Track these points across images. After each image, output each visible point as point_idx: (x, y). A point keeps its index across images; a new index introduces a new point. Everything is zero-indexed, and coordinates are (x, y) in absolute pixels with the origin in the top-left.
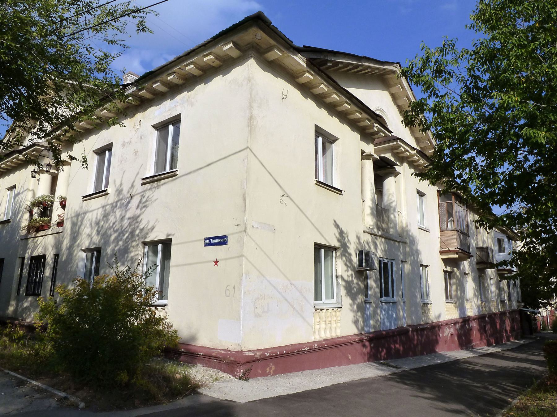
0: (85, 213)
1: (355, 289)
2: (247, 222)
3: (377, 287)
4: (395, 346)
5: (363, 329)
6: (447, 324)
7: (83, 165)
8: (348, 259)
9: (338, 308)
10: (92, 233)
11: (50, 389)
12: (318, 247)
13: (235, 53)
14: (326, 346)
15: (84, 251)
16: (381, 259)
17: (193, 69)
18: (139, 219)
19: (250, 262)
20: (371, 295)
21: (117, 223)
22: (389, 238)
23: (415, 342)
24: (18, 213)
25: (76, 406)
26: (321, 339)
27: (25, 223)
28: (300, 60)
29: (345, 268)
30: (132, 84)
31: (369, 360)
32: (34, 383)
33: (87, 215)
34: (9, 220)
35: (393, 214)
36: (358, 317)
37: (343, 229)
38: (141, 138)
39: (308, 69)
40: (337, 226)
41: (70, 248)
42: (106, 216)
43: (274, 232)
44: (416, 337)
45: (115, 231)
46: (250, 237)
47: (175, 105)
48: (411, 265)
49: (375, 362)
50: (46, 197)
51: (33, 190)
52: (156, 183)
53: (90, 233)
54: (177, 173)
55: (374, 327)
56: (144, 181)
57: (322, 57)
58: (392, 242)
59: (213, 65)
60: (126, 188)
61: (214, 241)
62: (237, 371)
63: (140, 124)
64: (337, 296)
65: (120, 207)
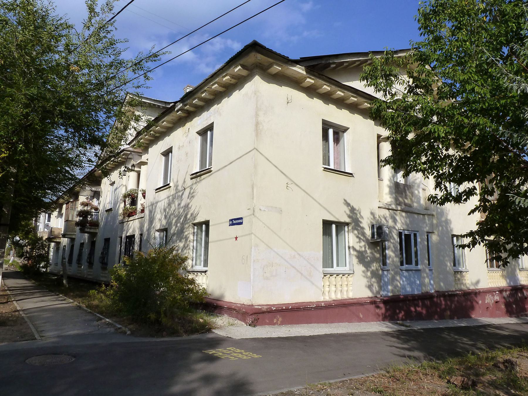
0: (157, 203)
1: (369, 258)
2: (254, 206)
3: (396, 256)
4: (416, 309)
5: (378, 292)
6: (490, 291)
7: (119, 177)
8: (360, 232)
9: (349, 274)
10: (161, 218)
11: (114, 324)
12: (327, 224)
13: (245, 73)
14: (334, 305)
15: (158, 231)
16: (401, 231)
17: (218, 88)
18: (190, 206)
19: (258, 238)
20: (389, 264)
21: (176, 210)
22: (411, 211)
23: (443, 306)
24: (117, 204)
25: (125, 333)
26: (330, 300)
27: (121, 211)
28: (300, 70)
29: (358, 240)
30: (179, 101)
31: (383, 320)
32: (107, 320)
33: (158, 203)
34: (112, 208)
35: (417, 190)
36: (372, 282)
37: (355, 207)
38: (190, 142)
39: (308, 76)
40: (348, 204)
41: (149, 230)
42: (169, 205)
43: (281, 213)
44: (443, 303)
45: (175, 217)
46: (258, 218)
47: (210, 116)
48: (438, 235)
49: (392, 322)
50: (133, 191)
51: (125, 185)
52: (199, 178)
53: (160, 218)
54: (212, 169)
55: (392, 291)
56: (192, 176)
57: (323, 62)
58: (416, 216)
59: (232, 82)
60: (180, 183)
61: (235, 222)
62: (248, 320)
63: (189, 132)
64: (349, 264)
65: (178, 198)
